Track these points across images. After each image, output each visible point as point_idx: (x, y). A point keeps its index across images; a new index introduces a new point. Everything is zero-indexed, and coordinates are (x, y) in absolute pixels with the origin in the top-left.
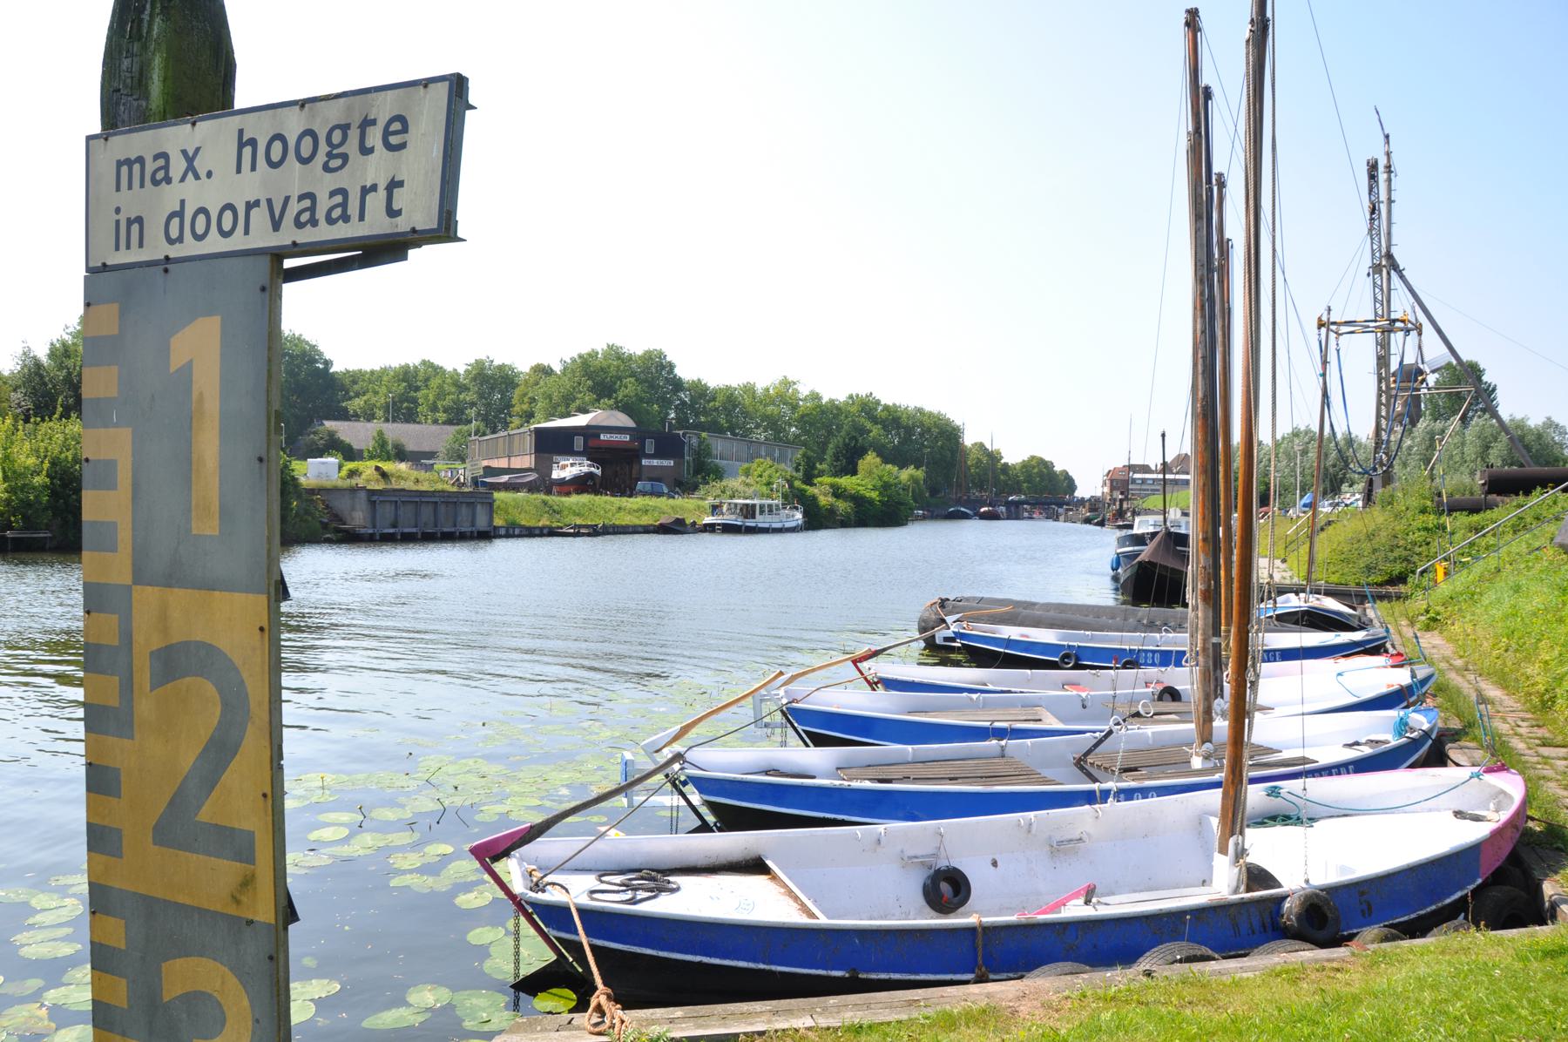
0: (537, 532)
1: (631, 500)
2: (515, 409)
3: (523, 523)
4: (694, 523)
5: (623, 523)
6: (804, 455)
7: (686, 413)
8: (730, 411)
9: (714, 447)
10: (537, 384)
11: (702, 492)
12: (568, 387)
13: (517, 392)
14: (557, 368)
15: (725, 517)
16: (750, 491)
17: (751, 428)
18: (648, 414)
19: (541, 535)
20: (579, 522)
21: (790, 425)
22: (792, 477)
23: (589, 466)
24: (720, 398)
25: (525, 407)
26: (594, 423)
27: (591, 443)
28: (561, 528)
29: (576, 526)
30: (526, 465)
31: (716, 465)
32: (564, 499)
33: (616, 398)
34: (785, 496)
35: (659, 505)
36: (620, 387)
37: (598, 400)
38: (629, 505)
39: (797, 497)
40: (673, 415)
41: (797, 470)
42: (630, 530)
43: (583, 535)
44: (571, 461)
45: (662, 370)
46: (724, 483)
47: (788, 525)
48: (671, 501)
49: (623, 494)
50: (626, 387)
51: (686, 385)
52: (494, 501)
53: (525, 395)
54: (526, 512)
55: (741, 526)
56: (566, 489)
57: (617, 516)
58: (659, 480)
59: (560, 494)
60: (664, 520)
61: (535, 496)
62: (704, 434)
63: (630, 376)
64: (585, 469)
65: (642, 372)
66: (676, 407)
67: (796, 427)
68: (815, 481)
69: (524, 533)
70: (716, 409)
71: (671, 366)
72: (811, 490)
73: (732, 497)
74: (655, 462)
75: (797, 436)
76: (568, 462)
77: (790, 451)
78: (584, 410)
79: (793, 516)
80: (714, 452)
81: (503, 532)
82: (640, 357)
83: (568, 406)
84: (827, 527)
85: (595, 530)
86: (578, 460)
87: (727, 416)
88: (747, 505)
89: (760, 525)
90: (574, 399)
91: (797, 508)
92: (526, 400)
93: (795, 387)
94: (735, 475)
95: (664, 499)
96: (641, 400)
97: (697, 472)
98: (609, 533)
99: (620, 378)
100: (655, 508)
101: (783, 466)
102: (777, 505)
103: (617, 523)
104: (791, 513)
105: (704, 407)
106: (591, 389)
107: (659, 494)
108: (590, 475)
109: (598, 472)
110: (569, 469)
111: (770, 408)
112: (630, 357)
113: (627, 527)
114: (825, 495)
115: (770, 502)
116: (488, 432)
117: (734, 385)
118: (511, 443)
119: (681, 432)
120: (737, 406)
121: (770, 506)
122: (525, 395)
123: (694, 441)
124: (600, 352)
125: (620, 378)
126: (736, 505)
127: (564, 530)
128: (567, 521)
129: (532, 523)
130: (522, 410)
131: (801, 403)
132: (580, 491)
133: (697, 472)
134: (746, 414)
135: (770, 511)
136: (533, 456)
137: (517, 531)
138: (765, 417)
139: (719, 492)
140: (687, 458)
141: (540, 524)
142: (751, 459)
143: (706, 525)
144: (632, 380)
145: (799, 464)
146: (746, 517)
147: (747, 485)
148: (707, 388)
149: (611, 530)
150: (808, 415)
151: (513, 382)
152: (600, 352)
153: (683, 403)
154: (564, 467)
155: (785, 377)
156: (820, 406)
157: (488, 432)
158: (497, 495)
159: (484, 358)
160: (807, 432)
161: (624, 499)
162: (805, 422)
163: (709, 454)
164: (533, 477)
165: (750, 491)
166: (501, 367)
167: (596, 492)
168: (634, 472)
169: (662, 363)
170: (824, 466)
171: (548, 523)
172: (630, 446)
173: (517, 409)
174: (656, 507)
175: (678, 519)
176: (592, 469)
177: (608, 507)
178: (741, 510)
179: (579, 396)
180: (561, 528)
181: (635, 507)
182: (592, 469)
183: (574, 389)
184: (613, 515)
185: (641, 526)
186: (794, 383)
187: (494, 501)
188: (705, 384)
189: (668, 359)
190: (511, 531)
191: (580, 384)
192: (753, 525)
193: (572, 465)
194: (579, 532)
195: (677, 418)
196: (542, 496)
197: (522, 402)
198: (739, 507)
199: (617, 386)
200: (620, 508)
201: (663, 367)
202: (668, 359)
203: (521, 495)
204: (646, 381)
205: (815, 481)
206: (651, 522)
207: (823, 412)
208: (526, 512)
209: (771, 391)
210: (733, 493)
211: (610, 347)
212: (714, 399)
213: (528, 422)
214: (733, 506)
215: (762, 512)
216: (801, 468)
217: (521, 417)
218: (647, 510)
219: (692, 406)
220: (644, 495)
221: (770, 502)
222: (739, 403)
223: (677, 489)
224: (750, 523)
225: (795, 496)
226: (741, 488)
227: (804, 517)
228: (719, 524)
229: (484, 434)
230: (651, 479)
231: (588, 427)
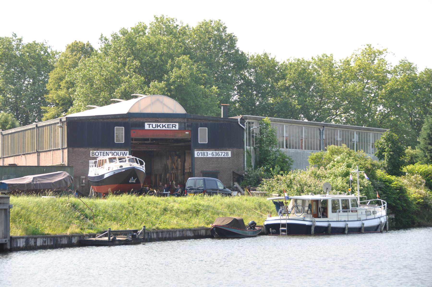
0: (65, 241)
1: (180, 199)
2: (50, 96)
3: (47, 231)
4: (253, 225)
5: (169, 227)
6: (389, 139)
7: (252, 95)
8: (303, 90)
9: (278, 134)
10: (75, 65)
11: (265, 187)
12: (110, 69)
13: (53, 75)
14: (97, 46)
15: (291, 216)
16: (321, 184)
17: (329, 109)
18: (207, 97)
19: (70, 245)
20: (115, 227)
21: (377, 103)
22: (373, 165)
23: (131, 160)
24: (291, 75)
25: (62, 93)
26: (136, 110)
27: (135, 134)
28: (94, 236)
29: (110, 233)
30: (58, 162)
31: (282, 155)
32: (252, 157)
33: (168, 80)
34: (364, 190)
35: (211, 204)
36: (172, 67)
37: (147, 83)
38: (176, 206)
39: (380, 188)
40: (236, 98)
41: (381, 157)
42: (178, 235)
43: (121, 243)
44: (110, 156)
45: (221, 45)
46: (291, 176)
47: (367, 224)
48: (227, 200)
49: (173, 193)
50: (180, 68)
51: (250, 62)
52: (10, 207)
53: (61, 79)
54: (52, 219)
55: (309, 227)
56: (104, 188)
57: (162, 218)
58: (215, 174)
59: (98, 195)
60: (219, 221)
61: (63, 199)
62: (267, 119)
63: (184, 54)
64: (127, 165)
65: (199, 48)
66: (239, 87)
67: (384, 106)
68: (404, 169)
69: (49, 243)
70: (287, 89)
71: (232, 40)
72: (402, 181)
73: (301, 191)
74: (210, 154)
75: (385, 116)
76: (107, 158)
77: (371, 134)
78: (127, 96)
79: (374, 213)
80: (279, 139)
81: (21, 243)
82: (194, 30)
83: (111, 91)
84: (420, 226)
85: (133, 236)
86: (120, 153)
87: (300, 95)
88: (317, 201)
89: (333, 225)
90: (119, 83)
91: (379, 203)
92: (63, 84)
93: (382, 56)
94: (303, 166)
95: (218, 197)
96: (197, 81)
97: (260, 163)
98: (151, 240)
99: (171, 57)
100: (207, 208)
101: (361, 153)
102: (355, 200)
103: (162, 227)
104: (372, 209)
105: (272, 87)
106: (139, 71)
107: (212, 192)
108: (132, 172)
109: (142, 168)
110: (107, 165)
111: (351, 85)
112: (184, 32)
113: (174, 231)
114: (417, 186)
115: (344, 196)
116: (17, 123)
117: (308, 58)
118: (40, 137)
119: (239, 118)
120: (311, 83)
121: (345, 201)
122: (61, 79)
123: (255, 127)
124: (149, 26)
125: (171, 57)
126: (304, 201)
127: (97, 239)
128: (101, 227)
129: (58, 231)
130: (58, 96)
131: (389, 76)
132: (118, 192)
133: (260, 163)
134: (322, 93)
135: (346, 208)
136: (66, 151)
137: (39, 242)
138: (345, 96)
139: (284, 187)
140: (247, 147)
141: (68, 232)
142: (322, 146)
143: (268, 226)
144: (186, 58)
145: (383, 150)
146: (316, 216)
147: (318, 177)
148: (274, 64)
149: (155, 236)
150: (397, 90)
151: (46, 64)
152: (149, 26)
153: (248, 83)
154: (101, 164)
155: (369, 46)
156: (413, 79)
157: (17, 123)
158: (13, 199)
159: (10, 36)
160: (398, 111)
161: (171, 199)
162: (395, 99)
163: (272, 142)
164: (63, 176)
165: (321, 184)
166: (31, 47)
167: (140, 192)
168: (187, 165)
169: (220, 36)
170: (417, 151)
171: (78, 230)
172: (179, 136)
173: (52, 96)
174: (208, 206)
175: (235, 220)
176: (135, 165)
177: (151, 208)
178: (310, 206)
179: (125, 78)
180: (94, 236)
181: (183, 207)
182: (135, 165)
183: (119, 70)
184: (157, 218)
185: (190, 230)
186: (380, 53)
187: (10, 207)
188: (273, 60)
189: (228, 31)
190: (32, 243)
191: (124, 64)
192: (325, 224)
193: (111, 160)
194: (114, 240)
195: (241, 101)
196: (73, 199)
197: (59, 87)
198: (307, 204)
199: (168, 66)
200: (165, 210)
201: (222, 41)
202: (228, 31)
203: (46, 199)
204: (203, 58)
205: (404, 169)
206: (202, 225)
207: (416, 86)
208: (52, 219)
209: (353, 64)
210: (412, 158)
211: (160, 20)
212: (284, 77)
213: (66, 111)
214: (300, 203)
215: (335, 209)
216: (385, 154)
217: (57, 105)
218: (198, 211)
219: (257, 86)
220: (195, 193)
221: (344, 196)
222: (314, 79)
223: (236, 184)
224: (321, 222)
225: (376, 188)
226: (311, 181)
227: (388, 214)
228: (283, 225)
229: (13, 126)
230: (205, 174)
231: (129, 115)
